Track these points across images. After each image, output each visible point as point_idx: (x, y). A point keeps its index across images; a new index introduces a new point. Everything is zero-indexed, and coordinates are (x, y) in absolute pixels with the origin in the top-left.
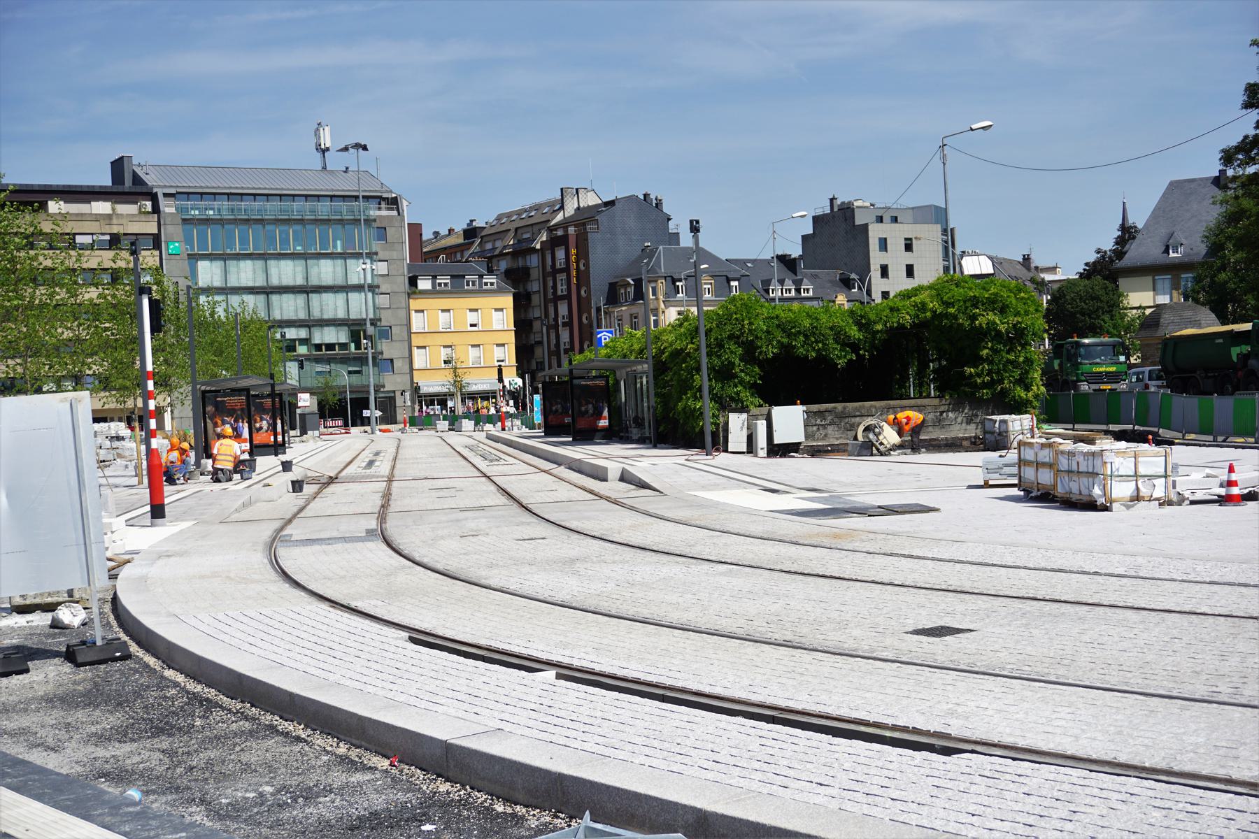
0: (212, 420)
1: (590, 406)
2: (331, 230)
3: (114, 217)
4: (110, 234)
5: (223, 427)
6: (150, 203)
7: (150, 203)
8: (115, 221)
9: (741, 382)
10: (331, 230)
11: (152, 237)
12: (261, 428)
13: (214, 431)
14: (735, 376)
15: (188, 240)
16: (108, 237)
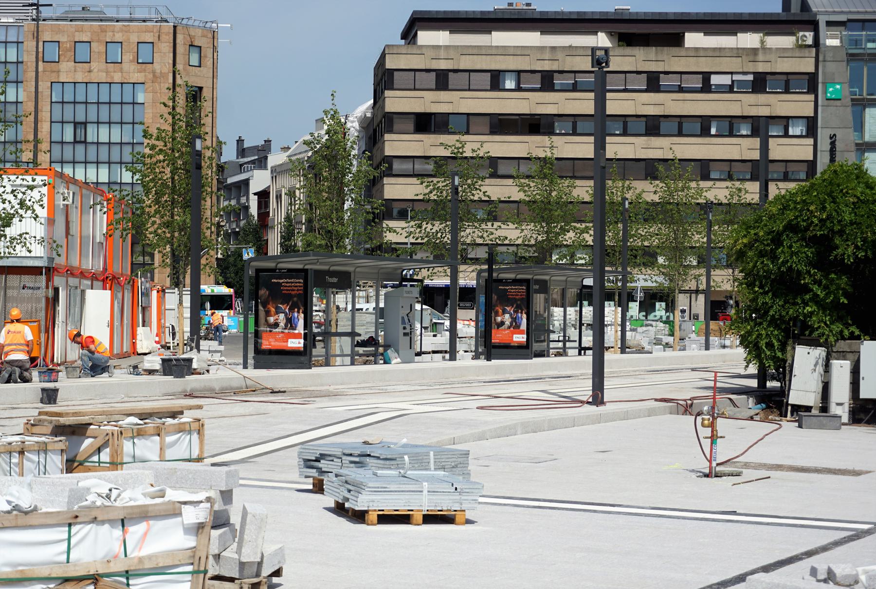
0: (264, 307)
1: (282, 316)
2: (865, 70)
3: (760, 52)
4: (754, 73)
5: (276, 317)
6: (812, 34)
7: (812, 34)
8: (761, 57)
9: (815, 299)
10: (865, 70)
11: (807, 77)
12: (502, 323)
13: (266, 320)
14: (806, 289)
15: (855, 81)
16: (750, 77)
